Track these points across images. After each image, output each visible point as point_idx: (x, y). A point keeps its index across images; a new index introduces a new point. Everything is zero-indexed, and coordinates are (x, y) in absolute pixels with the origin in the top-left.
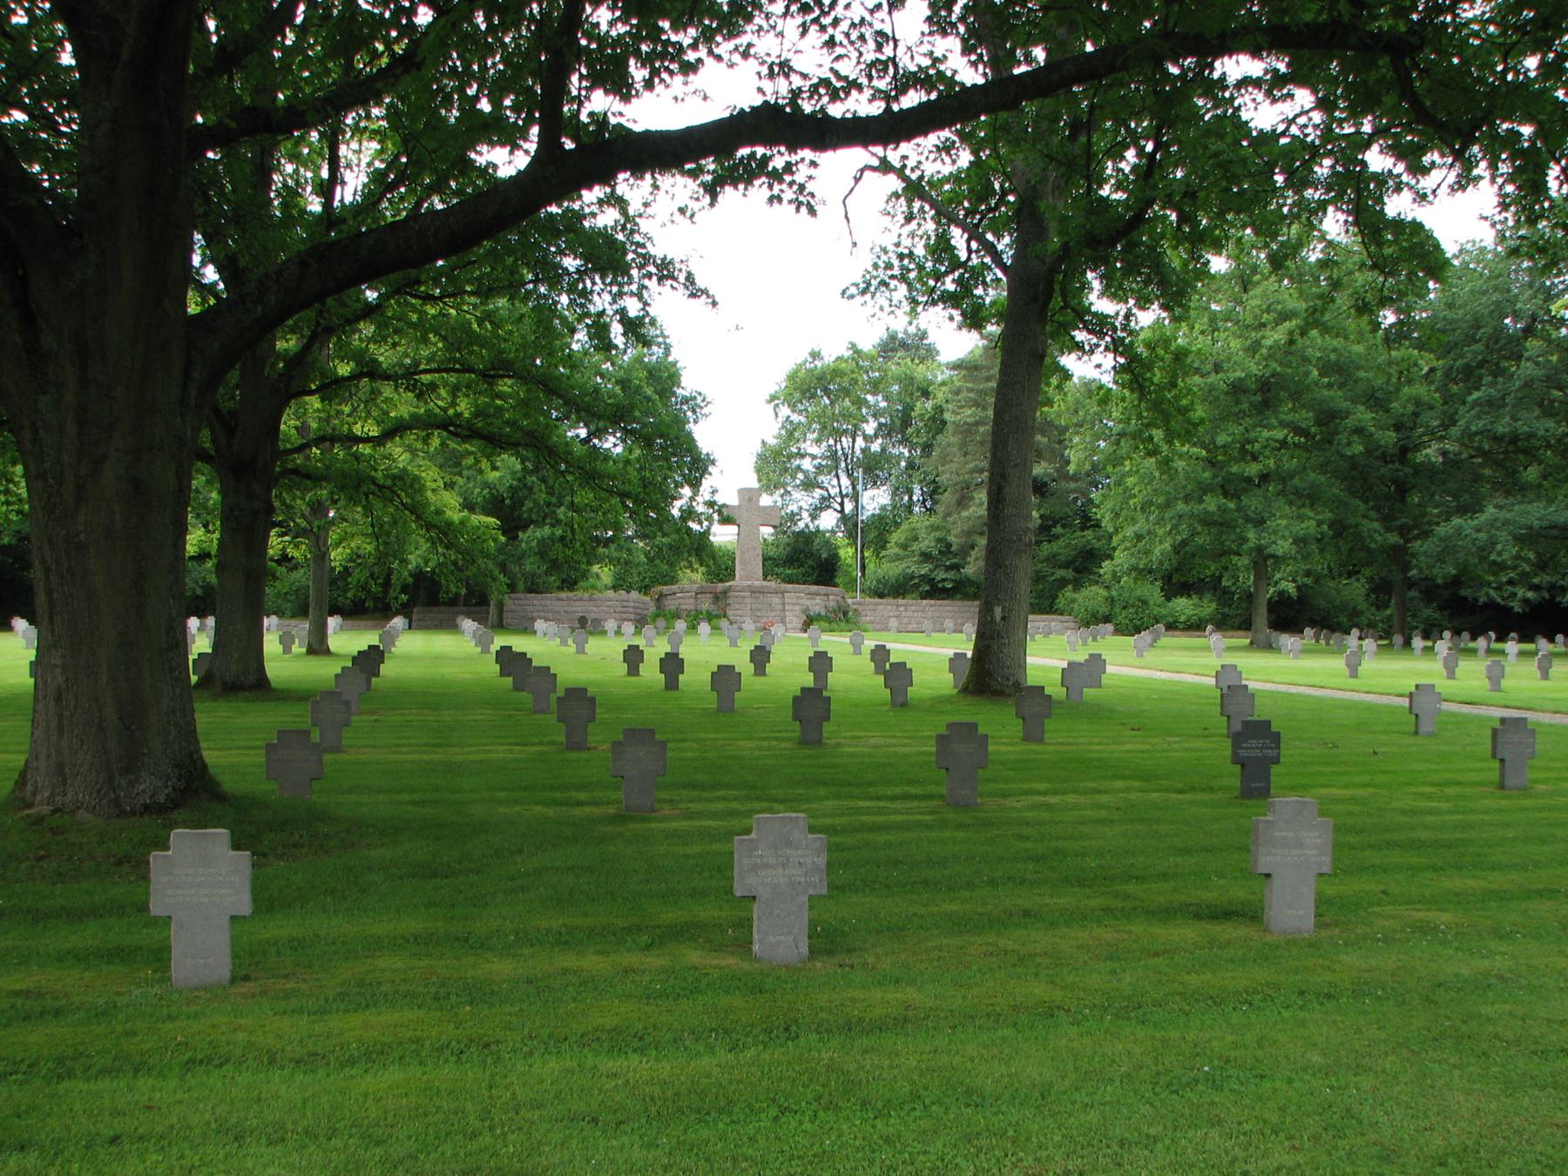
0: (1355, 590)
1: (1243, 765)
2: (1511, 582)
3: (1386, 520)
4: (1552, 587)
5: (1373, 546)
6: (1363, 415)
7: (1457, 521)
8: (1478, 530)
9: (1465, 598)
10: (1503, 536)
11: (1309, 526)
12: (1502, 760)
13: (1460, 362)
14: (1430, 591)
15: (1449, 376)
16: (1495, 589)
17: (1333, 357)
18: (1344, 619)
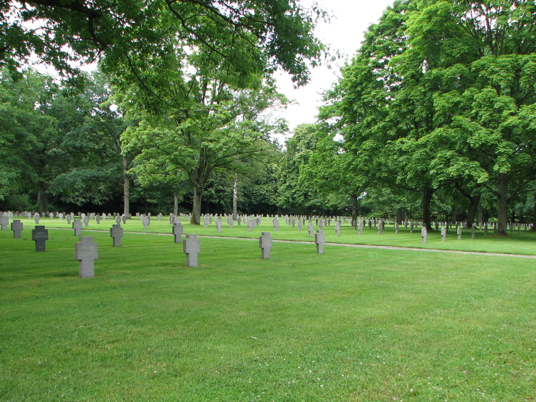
0: (25, 198)
1: (36, 241)
2: (78, 196)
3: (40, 173)
4: (90, 197)
5: (35, 182)
6: (32, 137)
7: (63, 174)
8: (71, 177)
9: (62, 201)
10: (79, 179)
11: (13, 174)
12: (114, 238)
13: (63, 122)
14: (50, 198)
15: (60, 126)
16: (72, 198)
17: (22, 116)
18: (21, 208)
